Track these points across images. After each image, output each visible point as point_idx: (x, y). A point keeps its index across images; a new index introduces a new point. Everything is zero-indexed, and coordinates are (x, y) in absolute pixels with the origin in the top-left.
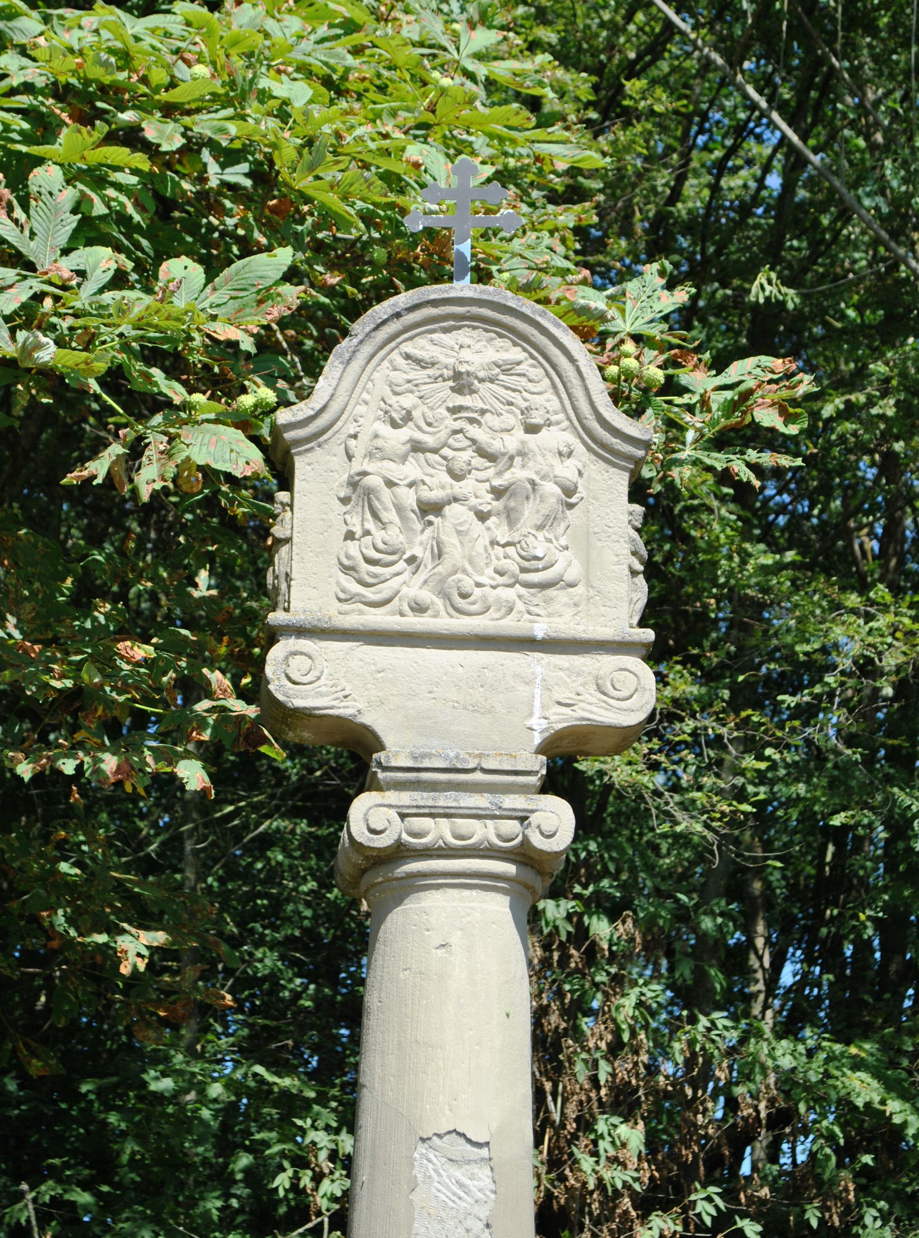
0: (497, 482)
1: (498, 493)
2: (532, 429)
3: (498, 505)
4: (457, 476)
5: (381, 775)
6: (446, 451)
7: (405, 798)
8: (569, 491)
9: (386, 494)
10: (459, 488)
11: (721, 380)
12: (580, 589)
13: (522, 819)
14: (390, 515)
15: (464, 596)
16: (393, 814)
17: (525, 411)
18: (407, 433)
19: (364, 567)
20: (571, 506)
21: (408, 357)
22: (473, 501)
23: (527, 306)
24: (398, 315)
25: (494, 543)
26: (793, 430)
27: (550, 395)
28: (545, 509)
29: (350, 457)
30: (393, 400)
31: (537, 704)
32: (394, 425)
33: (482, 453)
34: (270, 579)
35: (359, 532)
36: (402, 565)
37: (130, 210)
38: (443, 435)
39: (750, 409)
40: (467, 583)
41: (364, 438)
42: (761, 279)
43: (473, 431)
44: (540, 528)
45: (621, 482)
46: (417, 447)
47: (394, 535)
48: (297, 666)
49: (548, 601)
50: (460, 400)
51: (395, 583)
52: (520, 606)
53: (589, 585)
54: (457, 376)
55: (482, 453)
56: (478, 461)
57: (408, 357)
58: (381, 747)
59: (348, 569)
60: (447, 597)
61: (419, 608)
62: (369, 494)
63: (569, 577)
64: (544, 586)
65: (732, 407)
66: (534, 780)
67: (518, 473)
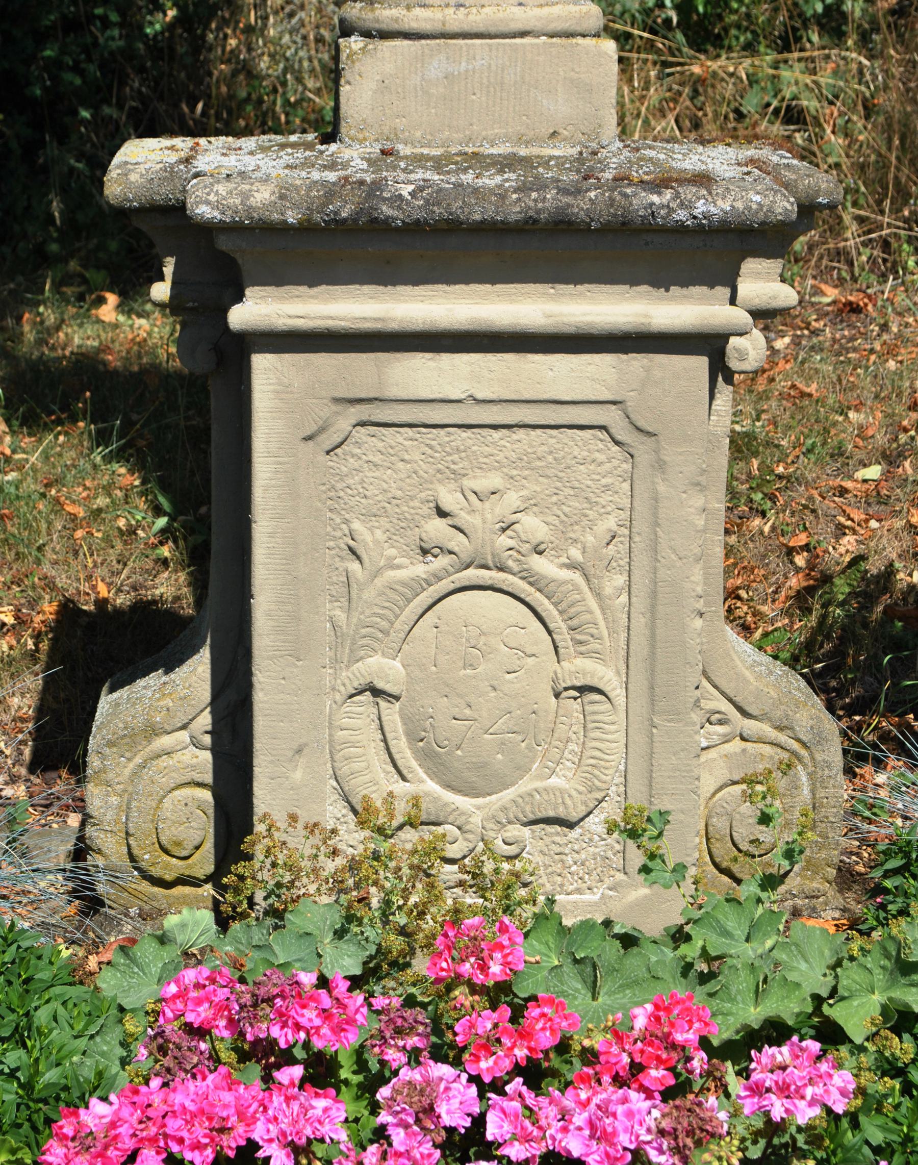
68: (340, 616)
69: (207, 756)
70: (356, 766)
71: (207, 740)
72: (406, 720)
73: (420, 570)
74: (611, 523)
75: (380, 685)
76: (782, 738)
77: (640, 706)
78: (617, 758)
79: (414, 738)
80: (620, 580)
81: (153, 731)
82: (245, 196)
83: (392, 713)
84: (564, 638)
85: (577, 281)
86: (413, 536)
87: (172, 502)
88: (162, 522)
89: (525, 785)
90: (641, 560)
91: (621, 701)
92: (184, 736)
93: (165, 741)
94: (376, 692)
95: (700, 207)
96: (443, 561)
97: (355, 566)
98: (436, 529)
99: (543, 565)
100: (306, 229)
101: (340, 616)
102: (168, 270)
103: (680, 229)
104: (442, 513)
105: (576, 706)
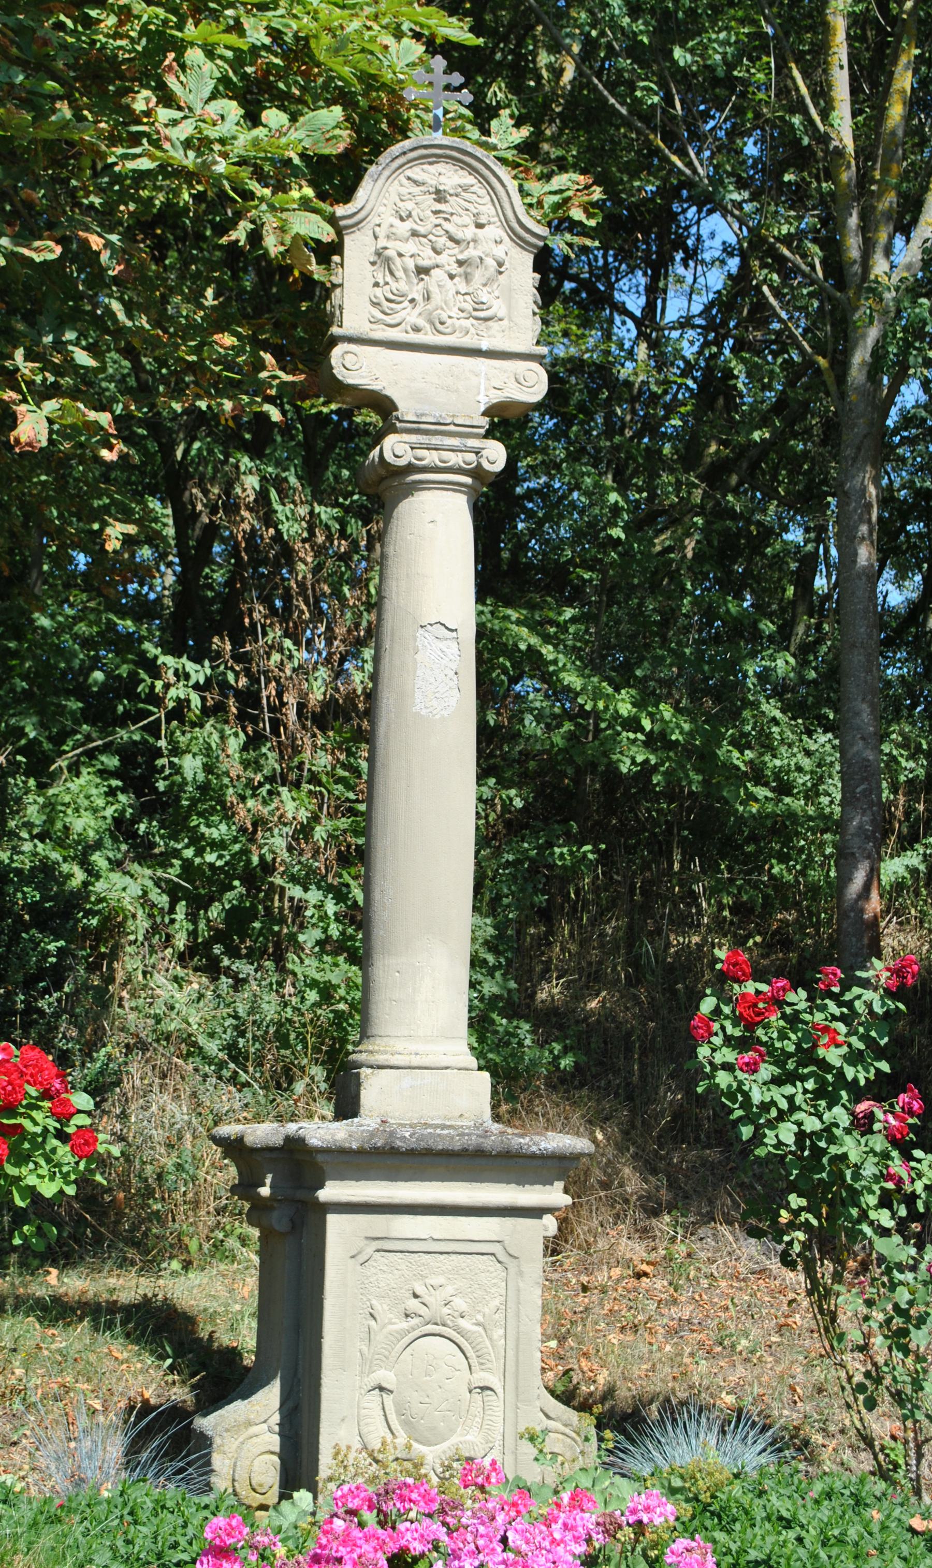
0: (460, 257)
1: (460, 263)
2: (480, 226)
3: (460, 270)
4: (437, 252)
5: (398, 425)
6: (431, 237)
7: (413, 438)
8: (500, 264)
9: (398, 260)
10: (440, 259)
11: (548, 188)
12: (505, 322)
13: (477, 453)
14: (400, 274)
15: (442, 323)
16: (407, 447)
17: (476, 215)
18: (409, 225)
19: (386, 304)
20: (501, 273)
21: (409, 178)
22: (447, 268)
23: (480, 152)
24: (404, 153)
25: (458, 293)
26: (592, 223)
27: (490, 206)
28: (487, 275)
29: (376, 238)
30: (400, 204)
31: (482, 388)
32: (402, 219)
33: (452, 239)
34: (328, 307)
35: (382, 283)
36: (406, 303)
37: (231, 74)
38: (429, 227)
39: (569, 209)
40: (444, 317)
41: (385, 226)
42: (494, 87)
43: (446, 225)
44: (485, 285)
45: (528, 259)
46: (415, 234)
47: (403, 286)
48: (349, 360)
49: (488, 328)
50: (439, 207)
51: (403, 314)
52: (472, 330)
53: (510, 320)
54: (438, 192)
55: (452, 239)
56: (450, 244)
57: (409, 178)
58: (396, 409)
59: (375, 304)
60: (432, 323)
61: (417, 329)
62: (388, 261)
63: (500, 315)
64: (486, 319)
65: (557, 207)
66: (482, 431)
67: (471, 253)
68: (365, 1349)
69: (277, 1438)
70: (371, 1428)
71: (277, 1428)
72: (396, 1404)
73: (404, 1325)
74: (496, 1302)
75: (384, 1385)
76: (567, 1431)
77: (510, 1397)
78: (499, 1426)
79: (400, 1414)
80: (502, 1332)
81: (249, 1424)
82: (333, 1135)
83: (388, 1399)
84: (474, 1361)
85: (482, 1181)
86: (401, 1308)
87: (173, 1350)
88: (169, 1361)
89: (454, 1440)
90: (511, 1323)
91: (501, 1394)
92: (265, 1426)
93: (254, 1430)
94: (382, 1389)
95: (543, 1145)
96: (416, 1321)
97: (373, 1323)
98: (413, 1304)
99: (464, 1323)
100: (360, 1152)
101: (365, 1349)
102: (268, 1181)
103: (533, 1156)
104: (416, 1296)
105: (479, 1397)
